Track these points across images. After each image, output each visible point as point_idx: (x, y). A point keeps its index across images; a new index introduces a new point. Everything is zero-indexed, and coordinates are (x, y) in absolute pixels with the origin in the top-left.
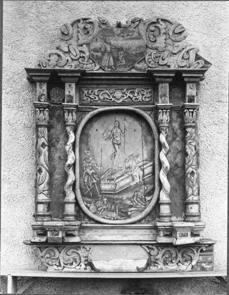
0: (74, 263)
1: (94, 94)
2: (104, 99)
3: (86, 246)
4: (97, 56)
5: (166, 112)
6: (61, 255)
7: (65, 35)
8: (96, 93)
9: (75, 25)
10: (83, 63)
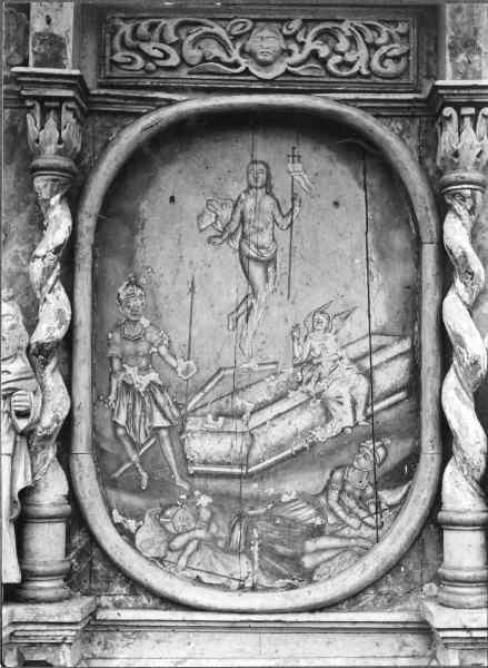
1: (162, 40)
2: (204, 60)
5: (474, 118)
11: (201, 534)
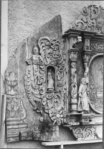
0: (89, 135)
1: (95, 46)
2: (100, 49)
3: (94, 126)
4: (100, 26)
5: (75, 53)
6: (83, 131)
7: (85, 13)
8: (97, 46)
9: (89, 8)
10: (94, 29)
11: (99, 106)
